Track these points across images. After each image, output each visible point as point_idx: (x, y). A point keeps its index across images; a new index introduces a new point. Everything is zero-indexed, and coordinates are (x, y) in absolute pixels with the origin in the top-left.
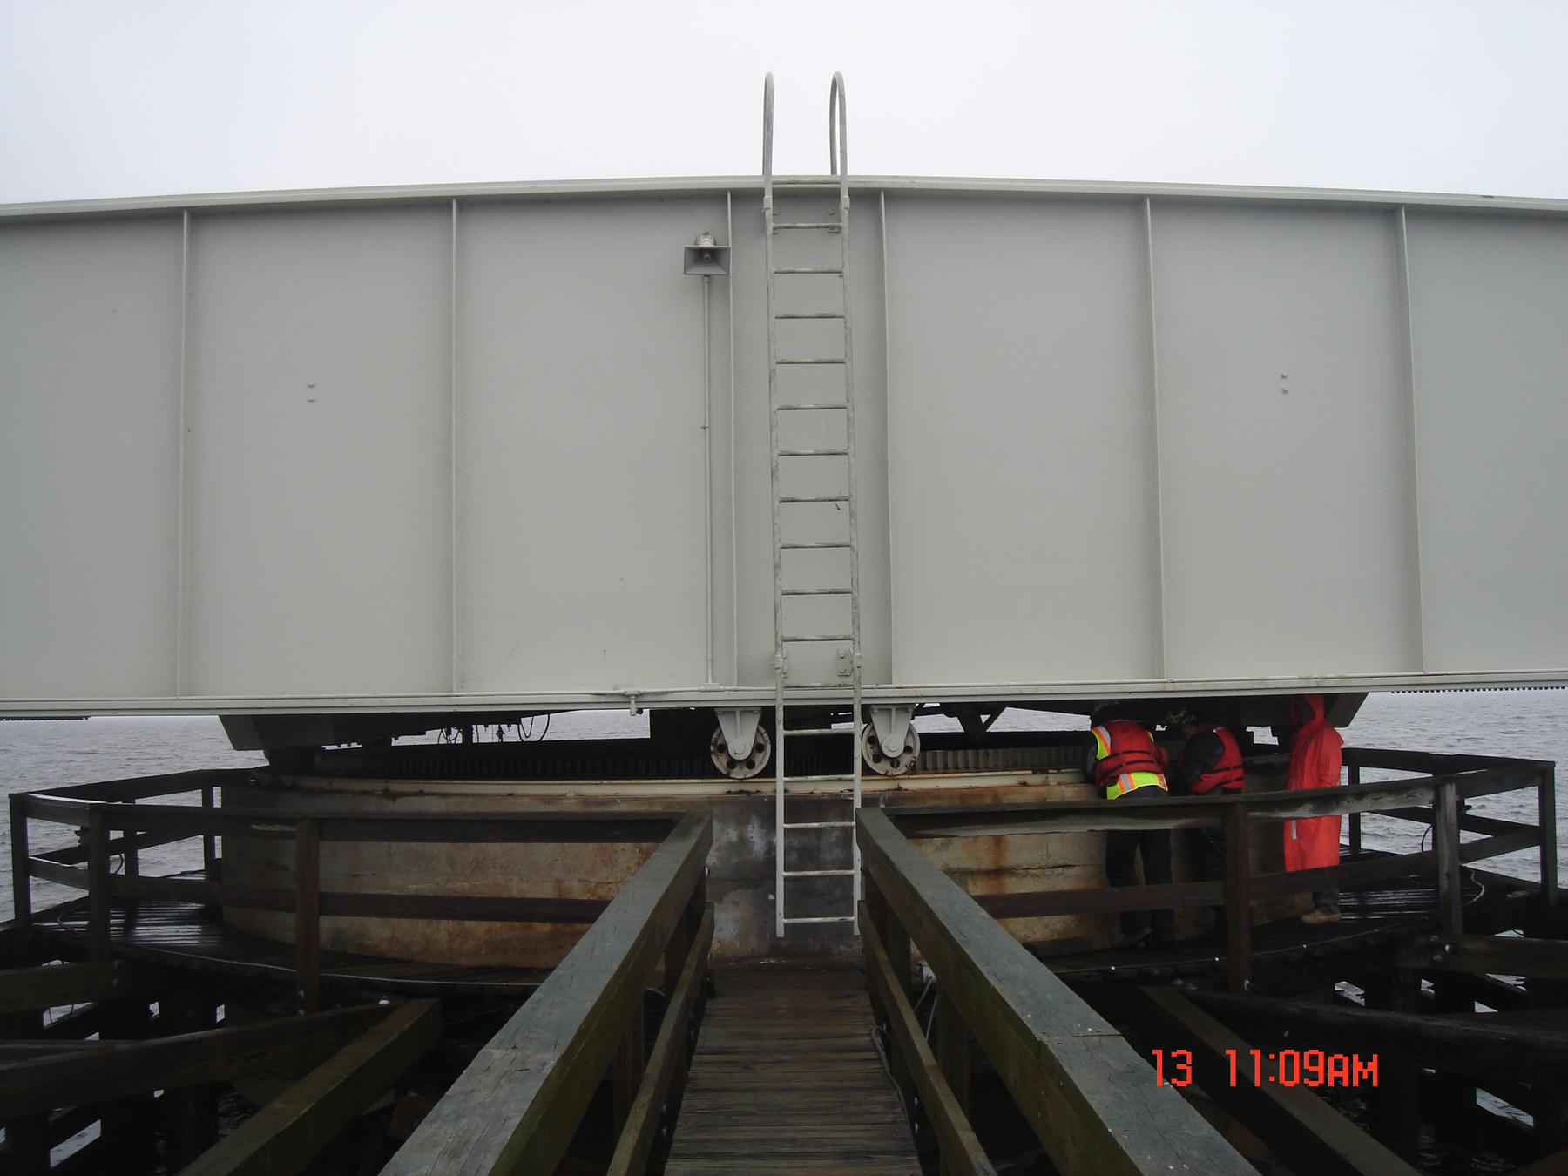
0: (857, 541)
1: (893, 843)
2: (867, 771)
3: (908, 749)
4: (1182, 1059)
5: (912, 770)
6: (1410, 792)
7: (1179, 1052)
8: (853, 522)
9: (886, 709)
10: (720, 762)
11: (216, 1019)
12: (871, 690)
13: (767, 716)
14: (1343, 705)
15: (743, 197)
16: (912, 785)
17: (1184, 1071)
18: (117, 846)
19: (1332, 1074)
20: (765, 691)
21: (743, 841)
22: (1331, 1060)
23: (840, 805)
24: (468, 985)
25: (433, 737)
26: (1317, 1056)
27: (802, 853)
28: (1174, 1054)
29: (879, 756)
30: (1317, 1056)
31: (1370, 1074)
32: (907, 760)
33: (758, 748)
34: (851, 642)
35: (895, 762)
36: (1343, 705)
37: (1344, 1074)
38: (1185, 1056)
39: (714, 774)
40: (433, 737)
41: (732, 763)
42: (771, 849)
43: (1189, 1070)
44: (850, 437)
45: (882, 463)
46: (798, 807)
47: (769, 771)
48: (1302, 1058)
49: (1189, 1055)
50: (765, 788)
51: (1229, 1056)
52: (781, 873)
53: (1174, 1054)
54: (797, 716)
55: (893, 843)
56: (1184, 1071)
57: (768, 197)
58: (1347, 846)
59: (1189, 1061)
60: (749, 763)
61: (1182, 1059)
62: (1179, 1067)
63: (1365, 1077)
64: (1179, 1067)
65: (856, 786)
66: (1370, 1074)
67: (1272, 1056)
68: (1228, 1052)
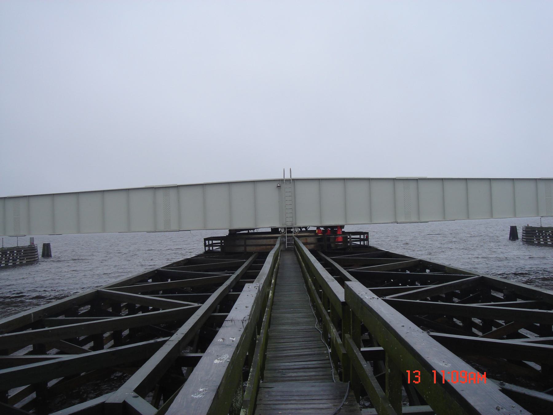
0: (293, 311)
1: (296, 239)
2: (294, 233)
3: (298, 231)
4: (417, 374)
5: (299, 233)
7: (416, 371)
9: (296, 228)
10: (281, 233)
11: (94, 343)
12: (295, 226)
13: (285, 228)
14: (342, 227)
15: (282, 180)
16: (298, 235)
18: (223, 243)
20: (285, 226)
21: (283, 240)
23: (292, 236)
25: (245, 232)
27: (288, 240)
28: (414, 372)
29: (295, 232)
32: (298, 232)
33: (284, 231)
35: (297, 232)
36: (342, 227)
38: (418, 373)
39: (280, 234)
40: (245, 232)
41: (282, 233)
42: (286, 240)
43: (419, 378)
44: (293, 220)
45: (295, 206)
46: (288, 237)
47: (285, 233)
50: (285, 235)
51: (433, 372)
52: (286, 242)
53: (414, 372)
54: (288, 228)
55: (296, 239)
57: (284, 181)
58: (305, 231)
59: (419, 374)
60: (283, 233)
61: (417, 374)
62: (416, 376)
64: (416, 376)
65: (293, 235)
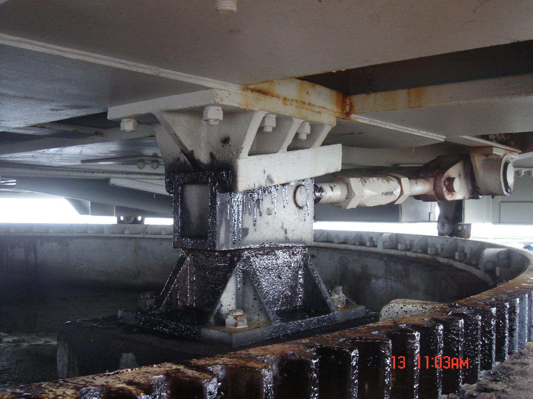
4: (402, 359)
6: (101, 235)
7: (401, 357)
8: (318, 110)
17: (447, 363)
19: (453, 364)
22: (452, 359)
24: (402, 122)
26: (456, 360)
28: (399, 358)
30: (456, 360)
31: (466, 364)
34: (431, 214)
37: (457, 364)
43: (404, 363)
48: (451, 360)
49: (404, 358)
53: (399, 358)
56: (447, 363)
59: (404, 360)
61: (402, 359)
62: (401, 362)
63: (464, 365)
64: (401, 362)
66: (466, 364)
67: (432, 358)
68: (426, 357)
